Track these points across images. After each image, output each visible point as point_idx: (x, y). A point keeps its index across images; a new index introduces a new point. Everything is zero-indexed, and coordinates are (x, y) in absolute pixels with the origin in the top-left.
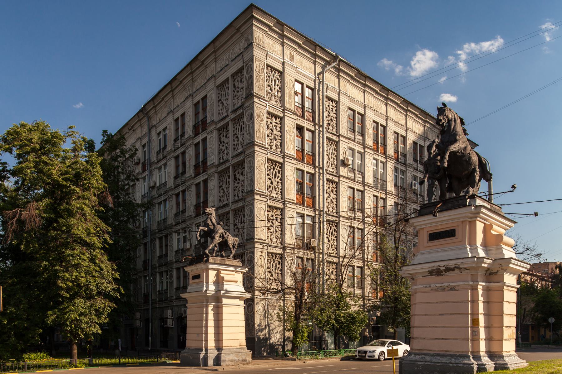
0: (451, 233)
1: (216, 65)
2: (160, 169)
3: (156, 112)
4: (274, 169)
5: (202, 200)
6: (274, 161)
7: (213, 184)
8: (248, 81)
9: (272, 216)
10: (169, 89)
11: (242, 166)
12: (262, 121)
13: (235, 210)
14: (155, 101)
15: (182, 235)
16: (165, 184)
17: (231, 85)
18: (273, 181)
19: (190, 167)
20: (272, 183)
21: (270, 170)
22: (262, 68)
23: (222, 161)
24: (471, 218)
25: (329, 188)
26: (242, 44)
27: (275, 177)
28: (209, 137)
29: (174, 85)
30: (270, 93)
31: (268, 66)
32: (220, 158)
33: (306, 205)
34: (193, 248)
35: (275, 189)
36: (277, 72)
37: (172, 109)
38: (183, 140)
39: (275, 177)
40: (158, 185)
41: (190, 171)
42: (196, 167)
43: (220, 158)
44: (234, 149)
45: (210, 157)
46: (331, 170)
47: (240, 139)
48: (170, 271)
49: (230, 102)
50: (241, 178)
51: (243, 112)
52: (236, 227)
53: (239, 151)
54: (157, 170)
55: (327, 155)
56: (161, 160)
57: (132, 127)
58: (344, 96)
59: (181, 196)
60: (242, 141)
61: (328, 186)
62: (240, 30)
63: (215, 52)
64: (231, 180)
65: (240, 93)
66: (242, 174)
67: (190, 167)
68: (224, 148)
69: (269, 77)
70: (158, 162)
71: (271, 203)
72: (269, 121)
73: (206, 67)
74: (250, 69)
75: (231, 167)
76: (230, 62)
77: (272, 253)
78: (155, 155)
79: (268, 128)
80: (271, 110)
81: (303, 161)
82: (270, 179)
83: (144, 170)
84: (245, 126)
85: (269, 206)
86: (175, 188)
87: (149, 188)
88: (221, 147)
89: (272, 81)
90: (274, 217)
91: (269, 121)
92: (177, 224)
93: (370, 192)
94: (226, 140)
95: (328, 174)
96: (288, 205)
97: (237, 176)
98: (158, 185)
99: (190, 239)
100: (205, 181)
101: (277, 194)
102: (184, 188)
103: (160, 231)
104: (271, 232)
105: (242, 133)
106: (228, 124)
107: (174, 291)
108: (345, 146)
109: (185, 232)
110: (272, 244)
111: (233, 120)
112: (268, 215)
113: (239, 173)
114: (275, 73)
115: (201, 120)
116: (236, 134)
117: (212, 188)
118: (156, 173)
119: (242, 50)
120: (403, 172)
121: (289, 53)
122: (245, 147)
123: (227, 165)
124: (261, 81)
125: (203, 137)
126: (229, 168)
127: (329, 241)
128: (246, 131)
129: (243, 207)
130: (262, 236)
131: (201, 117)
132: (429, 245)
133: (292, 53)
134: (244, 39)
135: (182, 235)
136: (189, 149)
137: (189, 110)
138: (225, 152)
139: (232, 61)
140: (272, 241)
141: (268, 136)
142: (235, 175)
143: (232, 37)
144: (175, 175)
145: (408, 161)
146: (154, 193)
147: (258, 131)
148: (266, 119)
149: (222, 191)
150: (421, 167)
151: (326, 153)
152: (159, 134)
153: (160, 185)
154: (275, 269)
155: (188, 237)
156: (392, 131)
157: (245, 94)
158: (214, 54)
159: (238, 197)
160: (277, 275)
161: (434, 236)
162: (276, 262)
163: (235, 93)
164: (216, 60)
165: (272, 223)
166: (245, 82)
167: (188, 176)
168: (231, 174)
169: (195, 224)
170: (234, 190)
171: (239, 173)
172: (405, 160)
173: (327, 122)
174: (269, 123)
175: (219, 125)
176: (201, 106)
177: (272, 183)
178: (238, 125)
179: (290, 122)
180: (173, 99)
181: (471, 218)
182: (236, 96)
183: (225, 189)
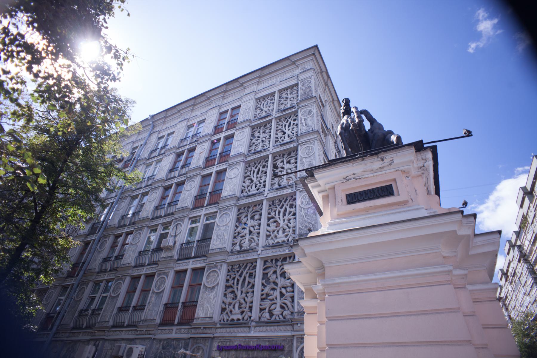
34: (178, 246)
38: (171, 210)
42: (170, 307)
54: (145, 166)
56: (105, 271)
63: (260, 77)
64: (258, 281)
73: (245, 88)
75: (270, 156)
86: (135, 267)
99: (175, 236)
107: (115, 311)
125: (219, 169)
138: (248, 237)
144: (170, 168)
149: (230, 296)
152: (160, 138)
169: (190, 218)
171: (275, 272)
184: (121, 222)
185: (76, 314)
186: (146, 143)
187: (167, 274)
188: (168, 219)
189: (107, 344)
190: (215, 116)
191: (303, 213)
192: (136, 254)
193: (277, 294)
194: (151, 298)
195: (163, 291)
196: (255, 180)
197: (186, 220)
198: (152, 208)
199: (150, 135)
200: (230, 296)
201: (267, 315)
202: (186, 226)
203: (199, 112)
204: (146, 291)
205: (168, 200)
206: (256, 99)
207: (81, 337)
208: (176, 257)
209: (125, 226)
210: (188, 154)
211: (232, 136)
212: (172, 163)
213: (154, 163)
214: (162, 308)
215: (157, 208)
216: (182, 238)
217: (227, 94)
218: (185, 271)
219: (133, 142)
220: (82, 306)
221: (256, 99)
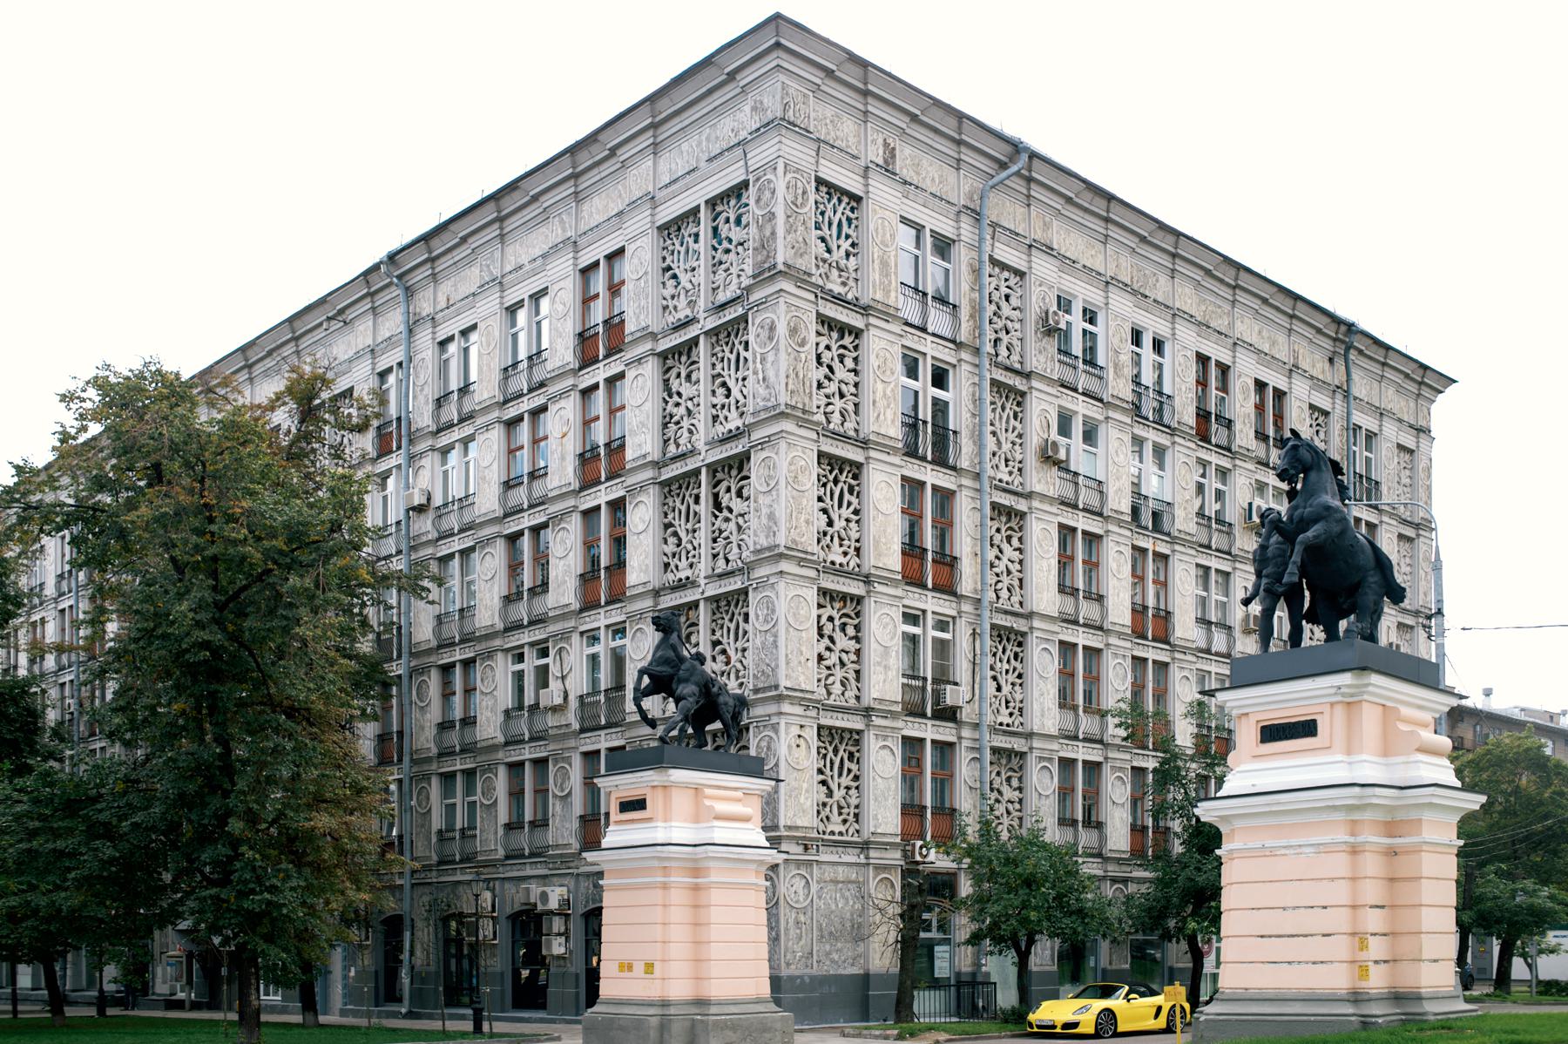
0: (1307, 729)
1: (655, 163)
2: (445, 452)
3: (434, 275)
4: (836, 481)
6: (838, 458)
7: (643, 517)
8: (760, 228)
9: (831, 619)
10: (489, 213)
11: (740, 469)
12: (802, 344)
13: (715, 600)
14: (434, 242)
15: (531, 663)
16: (465, 502)
17: (704, 228)
18: (835, 517)
19: (563, 458)
20: (830, 524)
21: (824, 485)
22: (804, 193)
23: (672, 450)
24: (1352, 695)
25: (998, 530)
26: (740, 115)
27: (840, 506)
29: (509, 204)
30: (824, 261)
31: (820, 182)
32: (666, 442)
33: (930, 585)
34: (573, 703)
35: (841, 539)
36: (846, 200)
37: (497, 272)
38: (538, 376)
39: (840, 506)
40: (438, 500)
43: (666, 442)
44: (715, 418)
46: (1006, 478)
47: (735, 392)
48: (484, 772)
49: (701, 277)
51: (746, 315)
52: (718, 648)
53: (732, 426)
54: (437, 456)
55: (994, 433)
56: (450, 426)
57: (342, 311)
58: (1045, 257)
59: (526, 542)
60: (740, 398)
61: (996, 525)
62: (738, 77)
64: (704, 508)
65: (732, 256)
66: (739, 494)
67: (563, 458)
68: (682, 410)
69: (822, 213)
70: (439, 431)
71: (830, 583)
72: (824, 341)
74: (767, 194)
75: (704, 470)
76: (703, 164)
77: (830, 728)
78: (431, 407)
79: (819, 363)
82: (825, 511)
83: (384, 450)
84: (749, 355)
85: (823, 592)
87: (408, 511)
88: (670, 408)
89: (830, 224)
90: (837, 623)
91: (824, 341)
92: (514, 627)
93: (1121, 540)
94: (687, 389)
95: (997, 487)
96: (879, 588)
98: (438, 500)
99: (563, 678)
100: (618, 506)
101: (845, 554)
102: (541, 519)
103: (513, 742)
104: (828, 668)
105: (740, 375)
106: (694, 342)
107: (501, 832)
108: (1045, 406)
109: (544, 653)
110: (831, 702)
111: (713, 333)
112: (819, 617)
113: (728, 490)
114: (840, 201)
116: (719, 375)
117: (641, 527)
118: (429, 462)
119: (743, 134)
120: (1223, 473)
121: (880, 141)
122: (749, 420)
123: (692, 464)
124: (801, 228)
127: (999, 689)
128: (756, 373)
129: (744, 592)
130: (802, 678)
131: (598, 313)
133: (890, 141)
134: (750, 103)
135: (531, 663)
136: (562, 403)
137: (561, 284)
138: (685, 423)
139: (710, 160)
140: (829, 694)
141: (820, 386)
142: (716, 496)
143: (710, 92)
145: (1238, 441)
146: (425, 526)
147: (793, 376)
148: (813, 338)
150: (1275, 456)
151: (991, 428)
152: (443, 344)
153: (445, 505)
154: (840, 775)
155: (554, 670)
156: (1189, 353)
157: (749, 261)
158: (650, 133)
159: (727, 561)
160: (843, 791)
161: (1273, 733)
162: (841, 753)
163: (719, 255)
164: (656, 148)
165: (831, 639)
167: (556, 483)
168: (704, 491)
169: (582, 633)
170: (715, 541)
172: (1231, 438)
173: (994, 336)
174: (821, 347)
175: (664, 345)
176: (600, 274)
177: (830, 524)
178: (727, 349)
179: (883, 344)
180: (502, 243)
181: (1352, 695)
182: (721, 263)
183: (682, 534)
184: (438, 416)
185: (434, 839)
187: (568, 760)
188: (538, 401)
189: (507, 885)
191: (758, 642)
193: (732, 526)
194: (555, 807)
195: (570, 793)
197: (575, 638)
198: (496, 603)
200: (672, 540)
201: (721, 563)
202: (577, 653)
203: (526, 247)
204: (541, 792)
207: (459, 877)
208: (576, 726)
214: (576, 824)
215: (508, 600)
216: (578, 683)
217: (585, 182)
218: (598, 508)
220: (437, 822)
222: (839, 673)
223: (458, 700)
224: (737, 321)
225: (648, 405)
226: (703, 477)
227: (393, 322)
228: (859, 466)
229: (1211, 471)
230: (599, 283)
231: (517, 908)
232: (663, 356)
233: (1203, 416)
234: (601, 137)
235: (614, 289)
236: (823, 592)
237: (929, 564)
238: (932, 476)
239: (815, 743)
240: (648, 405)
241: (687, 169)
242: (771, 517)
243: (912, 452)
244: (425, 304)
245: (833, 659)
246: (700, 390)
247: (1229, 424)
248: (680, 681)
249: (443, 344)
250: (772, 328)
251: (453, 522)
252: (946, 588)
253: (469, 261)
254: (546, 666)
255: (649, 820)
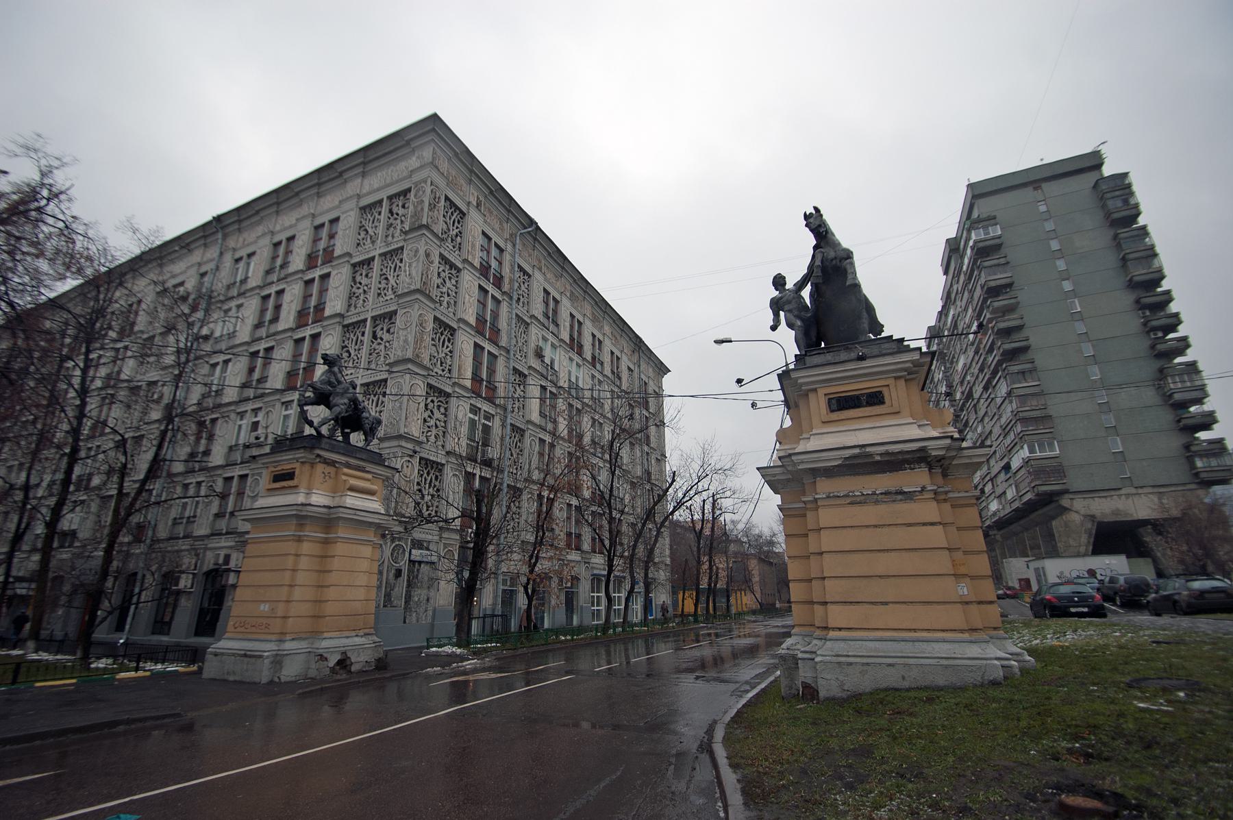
5: (313, 302)
8: (415, 207)
28: (333, 273)
29: (283, 197)
32: (350, 306)
41: (288, 318)
43: (350, 306)
45: (331, 300)
47: (392, 281)
50: (386, 337)
57: (188, 244)
63: (364, 164)
73: (346, 181)
77: (427, 460)
80: (446, 254)
81: (482, 334)
97: (379, 334)
98: (217, 334)
103: (230, 464)
107: (211, 518)
115: (324, 250)
125: (313, 332)
126: (365, 320)
131: (322, 245)
132: (835, 416)
138: (362, 297)
142: (374, 333)
144: (256, 322)
155: (262, 423)
166: (411, 207)
185: (170, 523)
186: (217, 268)
190: (307, 232)
192: (226, 450)
193: (382, 347)
196: (370, 230)
197: (278, 405)
199: (221, 254)
203: (287, 219)
205: (256, 375)
206: (361, 209)
209: (233, 298)
210: (288, 246)
211: (328, 275)
212: (257, 313)
213: (234, 310)
217: (323, 188)
219: (200, 264)
221: (361, 209)
222: (434, 431)
223: (203, 442)
224: (397, 249)
225: (341, 288)
226: (368, 323)
227: (213, 253)
228: (454, 330)
229: (596, 381)
230: (324, 233)
231: (211, 567)
232: (354, 265)
233: (594, 358)
234: (336, 166)
235: (332, 236)
236: (430, 386)
237: (483, 387)
238: (488, 346)
239: (417, 468)
240: (341, 288)
241: (378, 184)
242: (406, 341)
243: (481, 333)
244: (231, 243)
245: (432, 423)
246: (373, 280)
247: (602, 364)
248: (337, 394)
249: (238, 260)
250: (417, 251)
251: (223, 346)
252: (490, 400)
253: (258, 223)
254: (258, 422)
255: (296, 487)
